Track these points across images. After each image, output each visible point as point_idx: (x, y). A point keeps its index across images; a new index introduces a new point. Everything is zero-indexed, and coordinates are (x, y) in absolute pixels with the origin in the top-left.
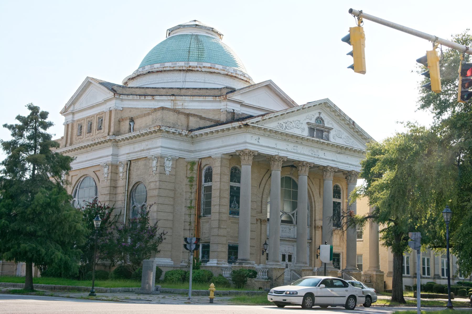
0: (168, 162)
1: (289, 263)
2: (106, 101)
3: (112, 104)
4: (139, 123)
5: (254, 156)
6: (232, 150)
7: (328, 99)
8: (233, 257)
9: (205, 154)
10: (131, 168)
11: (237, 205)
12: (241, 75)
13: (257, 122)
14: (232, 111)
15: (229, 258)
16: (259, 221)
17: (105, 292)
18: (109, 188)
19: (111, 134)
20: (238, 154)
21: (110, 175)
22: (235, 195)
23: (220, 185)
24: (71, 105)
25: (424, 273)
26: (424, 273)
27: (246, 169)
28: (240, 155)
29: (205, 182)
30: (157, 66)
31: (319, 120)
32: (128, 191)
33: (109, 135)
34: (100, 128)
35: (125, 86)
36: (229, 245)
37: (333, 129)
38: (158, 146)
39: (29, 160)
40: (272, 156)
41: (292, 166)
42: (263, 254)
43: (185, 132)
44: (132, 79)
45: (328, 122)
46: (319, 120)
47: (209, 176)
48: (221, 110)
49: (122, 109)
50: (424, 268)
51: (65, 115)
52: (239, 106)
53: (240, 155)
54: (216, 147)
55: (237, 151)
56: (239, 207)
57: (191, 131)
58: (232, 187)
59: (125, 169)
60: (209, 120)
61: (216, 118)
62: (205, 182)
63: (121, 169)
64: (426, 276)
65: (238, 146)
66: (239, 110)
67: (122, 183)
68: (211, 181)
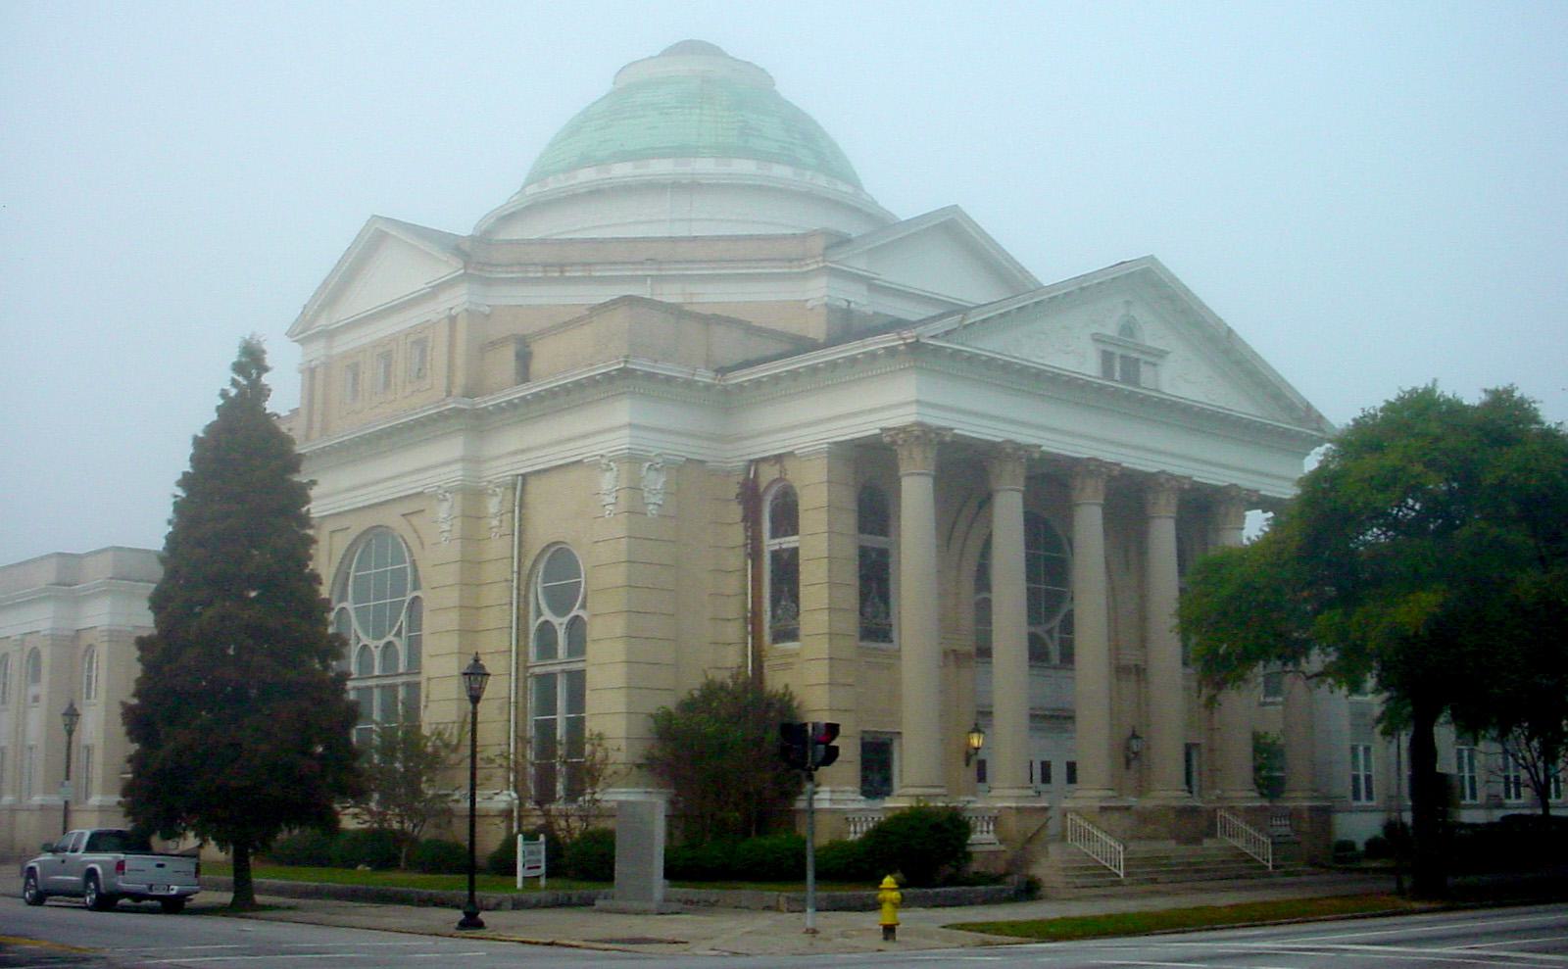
0: (652, 475)
1: (1043, 787)
2: (436, 290)
3: (458, 299)
4: (545, 355)
5: (942, 443)
6: (866, 427)
7: (1152, 257)
8: (878, 777)
9: (774, 446)
10: (530, 499)
11: (882, 607)
12: (31, 758)
13: (947, 333)
14: (844, 305)
15: (865, 780)
16: (952, 657)
17: (494, 909)
18: (458, 565)
19: (455, 391)
20: (887, 440)
21: (458, 523)
22: (874, 577)
23: (820, 545)
24: (322, 308)
25: (1356, 796)
26: (1356, 796)
27: (916, 498)
28: (894, 443)
29: (774, 535)
30: (586, 176)
31: (1128, 328)
32: (519, 573)
33: (449, 394)
34: (420, 374)
35: (483, 239)
36: (862, 739)
37: (1168, 353)
38: (609, 430)
39: (354, 688)
40: (994, 445)
41: (1052, 483)
42: (967, 765)
43: (705, 377)
44: (508, 218)
45: (1152, 333)
46: (1128, 328)
47: (787, 518)
48: (809, 305)
49: (487, 310)
50: (1356, 779)
51: (302, 342)
52: (863, 289)
53: (894, 443)
54: (808, 428)
55: (883, 430)
56: (888, 615)
57: (722, 371)
58: (864, 553)
59: (508, 505)
60: (773, 334)
61: (795, 327)
62: (774, 535)
63: (493, 505)
64: (1363, 802)
65: (886, 414)
66: (862, 301)
67: (498, 546)
68: (795, 532)
